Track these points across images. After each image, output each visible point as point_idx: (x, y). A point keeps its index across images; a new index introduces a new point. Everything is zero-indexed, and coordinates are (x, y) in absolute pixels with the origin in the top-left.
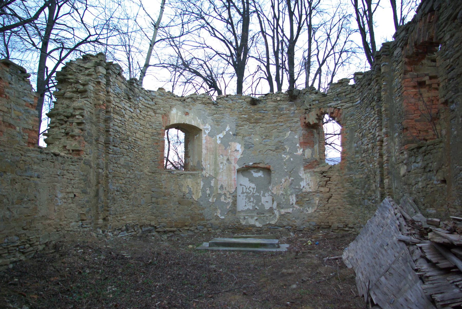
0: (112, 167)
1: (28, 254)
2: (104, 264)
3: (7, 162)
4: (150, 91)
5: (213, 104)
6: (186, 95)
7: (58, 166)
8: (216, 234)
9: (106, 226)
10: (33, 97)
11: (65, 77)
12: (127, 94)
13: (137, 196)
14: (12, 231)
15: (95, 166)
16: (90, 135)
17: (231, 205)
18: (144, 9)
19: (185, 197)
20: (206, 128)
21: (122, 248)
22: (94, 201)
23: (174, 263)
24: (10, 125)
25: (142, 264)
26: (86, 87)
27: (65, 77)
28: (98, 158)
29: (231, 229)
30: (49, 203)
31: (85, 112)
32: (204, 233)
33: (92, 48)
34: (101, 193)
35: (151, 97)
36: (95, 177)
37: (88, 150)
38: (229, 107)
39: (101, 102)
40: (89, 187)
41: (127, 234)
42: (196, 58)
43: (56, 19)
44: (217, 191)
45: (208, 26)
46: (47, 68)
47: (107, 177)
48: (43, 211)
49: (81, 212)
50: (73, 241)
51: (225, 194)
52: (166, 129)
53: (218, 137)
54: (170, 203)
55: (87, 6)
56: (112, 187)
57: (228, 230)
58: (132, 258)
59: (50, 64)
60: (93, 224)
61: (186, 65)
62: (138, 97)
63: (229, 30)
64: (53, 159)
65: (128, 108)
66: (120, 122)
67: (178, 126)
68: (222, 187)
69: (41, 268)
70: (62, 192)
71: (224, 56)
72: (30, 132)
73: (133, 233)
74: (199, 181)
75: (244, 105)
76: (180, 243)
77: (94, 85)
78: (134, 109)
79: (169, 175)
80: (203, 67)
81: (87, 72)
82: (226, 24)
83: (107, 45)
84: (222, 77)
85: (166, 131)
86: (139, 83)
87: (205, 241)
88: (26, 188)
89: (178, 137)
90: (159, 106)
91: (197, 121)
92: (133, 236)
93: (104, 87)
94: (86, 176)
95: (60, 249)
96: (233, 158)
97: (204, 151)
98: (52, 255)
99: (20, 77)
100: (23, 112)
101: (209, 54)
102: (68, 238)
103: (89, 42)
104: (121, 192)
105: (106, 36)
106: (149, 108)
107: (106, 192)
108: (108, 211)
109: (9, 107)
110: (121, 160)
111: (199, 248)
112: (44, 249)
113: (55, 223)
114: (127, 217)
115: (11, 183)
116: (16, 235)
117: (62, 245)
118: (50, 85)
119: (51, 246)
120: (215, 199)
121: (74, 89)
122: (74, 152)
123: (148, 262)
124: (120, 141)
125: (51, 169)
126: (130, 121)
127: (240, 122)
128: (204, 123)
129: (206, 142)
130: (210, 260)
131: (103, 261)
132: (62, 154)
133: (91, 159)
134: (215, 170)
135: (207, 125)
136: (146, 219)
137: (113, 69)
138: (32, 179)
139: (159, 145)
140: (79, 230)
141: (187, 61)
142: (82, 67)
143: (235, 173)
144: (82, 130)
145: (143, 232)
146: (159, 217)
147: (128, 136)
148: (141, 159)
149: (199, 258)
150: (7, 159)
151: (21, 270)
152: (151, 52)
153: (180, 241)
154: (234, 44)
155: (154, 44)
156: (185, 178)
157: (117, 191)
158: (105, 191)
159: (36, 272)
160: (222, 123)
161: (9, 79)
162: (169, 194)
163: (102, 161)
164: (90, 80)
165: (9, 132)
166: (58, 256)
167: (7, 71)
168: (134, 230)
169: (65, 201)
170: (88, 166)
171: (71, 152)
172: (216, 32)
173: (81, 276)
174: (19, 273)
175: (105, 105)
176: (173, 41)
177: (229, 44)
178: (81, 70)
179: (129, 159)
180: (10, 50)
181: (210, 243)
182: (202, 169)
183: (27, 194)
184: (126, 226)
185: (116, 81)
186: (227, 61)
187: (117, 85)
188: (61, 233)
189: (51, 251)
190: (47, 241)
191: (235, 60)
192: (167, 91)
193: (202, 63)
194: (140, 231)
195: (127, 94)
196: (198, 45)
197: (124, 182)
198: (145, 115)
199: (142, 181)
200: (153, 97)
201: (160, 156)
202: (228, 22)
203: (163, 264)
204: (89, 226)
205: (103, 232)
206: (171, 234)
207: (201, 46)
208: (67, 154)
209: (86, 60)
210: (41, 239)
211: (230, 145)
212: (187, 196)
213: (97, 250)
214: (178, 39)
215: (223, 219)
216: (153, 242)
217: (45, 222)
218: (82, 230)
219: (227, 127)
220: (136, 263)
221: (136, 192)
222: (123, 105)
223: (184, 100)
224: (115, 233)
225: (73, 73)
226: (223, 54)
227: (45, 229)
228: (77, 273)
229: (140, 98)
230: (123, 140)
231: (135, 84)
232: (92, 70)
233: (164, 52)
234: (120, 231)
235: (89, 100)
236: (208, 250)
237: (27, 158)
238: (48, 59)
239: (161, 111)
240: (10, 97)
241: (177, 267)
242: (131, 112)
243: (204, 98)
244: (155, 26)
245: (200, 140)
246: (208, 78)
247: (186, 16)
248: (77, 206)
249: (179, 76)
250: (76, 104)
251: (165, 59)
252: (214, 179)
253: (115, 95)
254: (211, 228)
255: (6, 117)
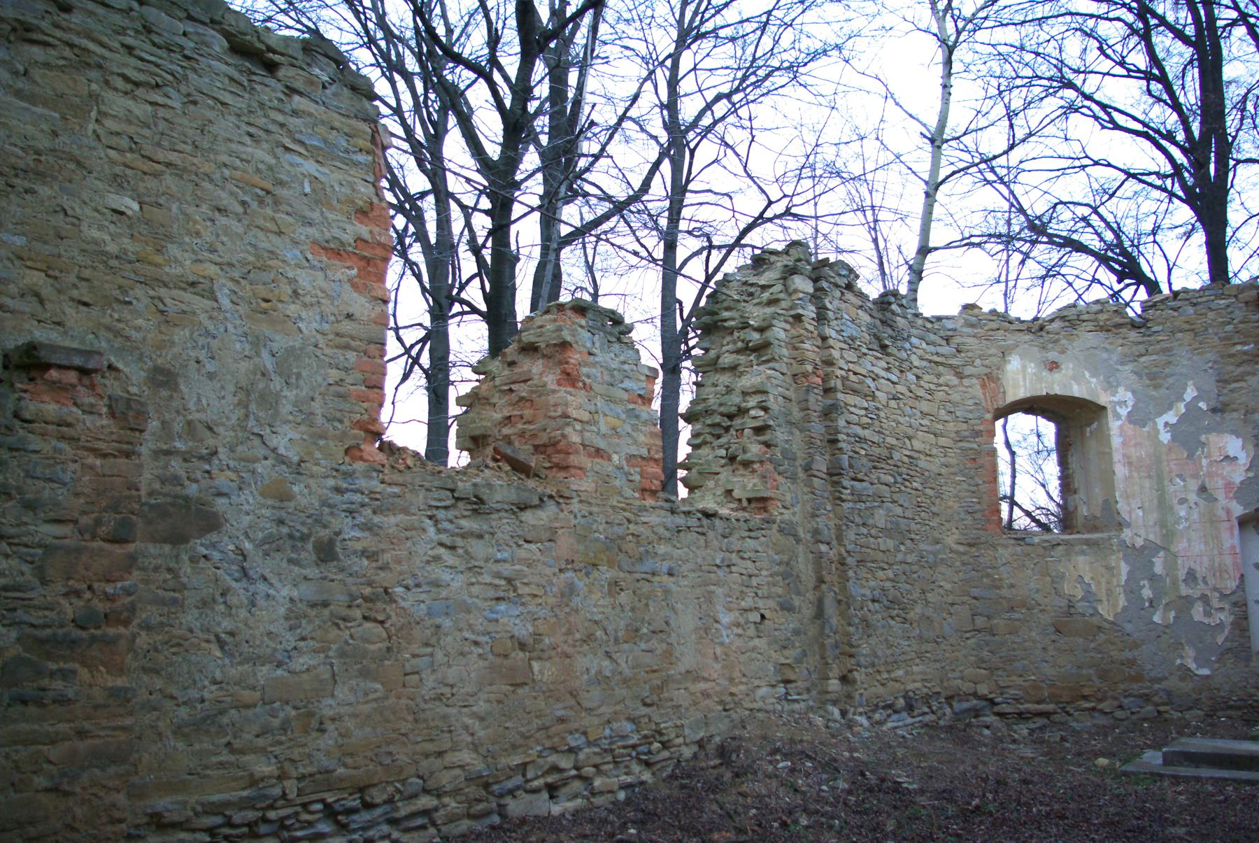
0: (853, 537)
1: (659, 766)
2: (845, 804)
3: (597, 540)
4: (939, 319)
5: (1133, 325)
6: (1047, 312)
7: (715, 542)
8: (1188, 725)
9: (850, 696)
10: (643, 378)
11: (716, 318)
12: (875, 335)
13: (929, 612)
14: (618, 708)
15: (809, 536)
16: (789, 456)
17: (1230, 633)
18: (897, 104)
19: (1072, 611)
20: (1119, 400)
21: (895, 762)
22: (812, 631)
23: (1048, 814)
24: (598, 452)
25: (951, 810)
26: (768, 334)
27: (716, 318)
28: (814, 516)
29: (1238, 708)
30: (701, 638)
31: (771, 397)
32: (1145, 720)
33: (779, 234)
34: (830, 608)
35: (942, 333)
36: (810, 567)
37: (788, 497)
38: (1187, 326)
39: (809, 368)
40: (798, 593)
41: (910, 721)
42: (1065, 203)
43: (688, 181)
44: (1177, 589)
45: (1087, 103)
46: (681, 303)
47: (842, 563)
48: (687, 660)
49: (783, 661)
50: (764, 738)
51: (1205, 599)
52: (997, 418)
53: (1160, 422)
54: (1031, 630)
55: (754, 132)
56: (860, 590)
57: (1229, 712)
58: (922, 792)
59: (686, 292)
60: (814, 693)
61: (1038, 228)
62: (907, 339)
63: (1159, 100)
64: (701, 526)
65: (883, 373)
66: (863, 412)
67: (1031, 406)
68: (1191, 576)
69: (690, 804)
70: (730, 610)
71: (1152, 179)
72: (644, 463)
73: (927, 718)
74: (1113, 560)
75: (1239, 315)
76: (1068, 750)
77: (788, 327)
78: (898, 373)
79: (1019, 549)
80: (1089, 225)
81: (766, 295)
82: (1144, 82)
83: (817, 218)
84: (1155, 242)
85: (1001, 421)
86: (904, 302)
87: (1150, 747)
88: (644, 601)
89: (1039, 436)
90: (970, 354)
91: (1090, 382)
92: (927, 725)
93: (811, 328)
94: (787, 564)
95: (734, 757)
96: (1221, 483)
97: (1120, 471)
98: (716, 772)
99: (611, 334)
100: (624, 416)
101: (1103, 181)
102: (752, 731)
103: (770, 220)
104: (886, 603)
105: (810, 195)
106: (942, 364)
107: (843, 607)
108: (852, 656)
109: (593, 408)
110: (876, 516)
111: (1129, 768)
112: (695, 756)
113: (718, 688)
114: (907, 673)
115: (610, 591)
116: (629, 719)
117: (739, 747)
118: (691, 343)
119: (711, 748)
120: (1172, 614)
121: (740, 344)
122: (753, 505)
123: (969, 804)
124: (870, 464)
125: (698, 552)
126: (893, 406)
127: (1231, 368)
128: (1111, 387)
129: (1124, 443)
130: (1167, 810)
131: (843, 795)
132: (724, 511)
133: (797, 519)
134: (1162, 524)
135: (1121, 390)
136: (962, 678)
137: (831, 277)
138: (657, 578)
139: (981, 462)
140: (779, 708)
141: (1038, 218)
142: (752, 285)
143: (1231, 528)
144: (768, 445)
145: (955, 713)
146: (1000, 673)
147: (891, 448)
148: (934, 509)
149: (1131, 800)
150: (597, 535)
151: (643, 806)
152: (931, 213)
153: (1068, 745)
154: (1180, 137)
155: (937, 189)
156: (1068, 554)
157: (873, 601)
158: (839, 602)
159: (677, 815)
160: (1170, 380)
161: (589, 345)
162: (1023, 604)
163: (826, 523)
164: (779, 315)
165: (597, 468)
166: (728, 776)
167: (581, 327)
168: (930, 707)
169: (740, 631)
170: (791, 538)
171: (745, 503)
172: (1115, 115)
173: (787, 834)
174: (640, 815)
175: (820, 372)
176: (992, 170)
177: (1164, 143)
178: (751, 294)
179: (899, 511)
180: (598, 275)
181: (1165, 754)
182: (1120, 525)
183: (647, 618)
184: (904, 697)
185: (843, 306)
186: (1164, 190)
187: (845, 316)
188: (734, 716)
189: (712, 763)
190: (702, 734)
191: (1190, 181)
192: (986, 309)
193: (1086, 211)
194: (948, 711)
195: (875, 335)
196: (1068, 163)
197: (891, 576)
198: (933, 387)
199: (942, 569)
200: (950, 333)
201: (985, 497)
202: (1148, 76)
203: (1015, 814)
204: (804, 697)
205: (844, 713)
206: (1040, 722)
207: (1077, 163)
208: (736, 510)
209: (761, 266)
210: (687, 731)
211: (1203, 445)
212: (1081, 606)
213: (827, 763)
214: (1002, 161)
215: (1207, 677)
216: (986, 745)
217: (692, 688)
218: (787, 707)
219: (1189, 390)
220: (933, 807)
221: (927, 602)
222: (869, 367)
223: (1041, 328)
224: (877, 716)
225: (732, 304)
226: (1150, 174)
227: (695, 704)
228: (776, 825)
229: (914, 340)
230: (877, 462)
231: (894, 307)
232: (778, 287)
233: (971, 204)
234: (889, 711)
235: (776, 365)
236: (1161, 776)
237: (641, 529)
238: (680, 280)
239: (978, 368)
240: (595, 386)
241: (1057, 825)
242: (893, 383)
243: (1101, 311)
244: (932, 141)
245: (1104, 438)
246: (1110, 254)
247: (1015, 92)
248: (769, 644)
249: (1023, 262)
250: (747, 382)
251: (977, 224)
252: (1162, 554)
253: (845, 342)
254: (1167, 704)
255: (587, 434)
